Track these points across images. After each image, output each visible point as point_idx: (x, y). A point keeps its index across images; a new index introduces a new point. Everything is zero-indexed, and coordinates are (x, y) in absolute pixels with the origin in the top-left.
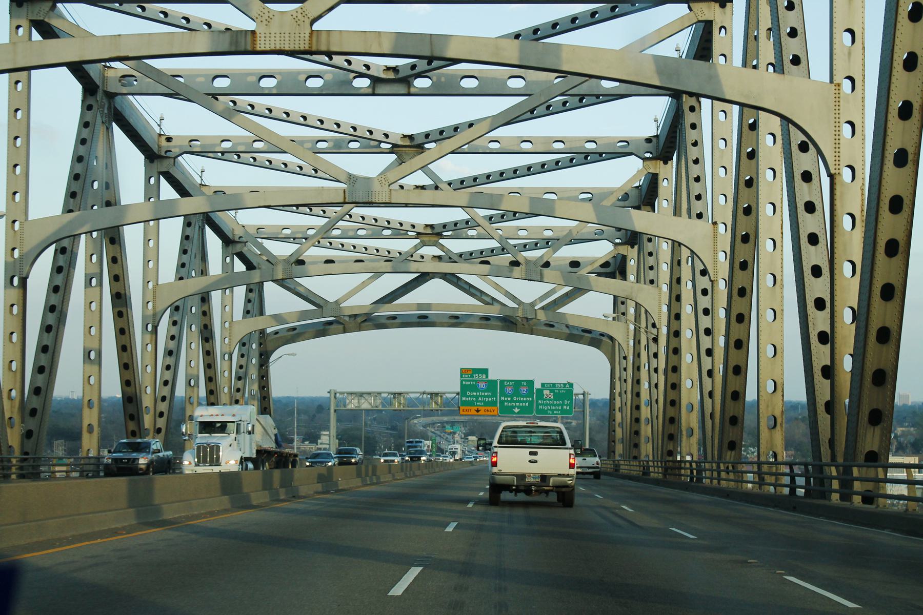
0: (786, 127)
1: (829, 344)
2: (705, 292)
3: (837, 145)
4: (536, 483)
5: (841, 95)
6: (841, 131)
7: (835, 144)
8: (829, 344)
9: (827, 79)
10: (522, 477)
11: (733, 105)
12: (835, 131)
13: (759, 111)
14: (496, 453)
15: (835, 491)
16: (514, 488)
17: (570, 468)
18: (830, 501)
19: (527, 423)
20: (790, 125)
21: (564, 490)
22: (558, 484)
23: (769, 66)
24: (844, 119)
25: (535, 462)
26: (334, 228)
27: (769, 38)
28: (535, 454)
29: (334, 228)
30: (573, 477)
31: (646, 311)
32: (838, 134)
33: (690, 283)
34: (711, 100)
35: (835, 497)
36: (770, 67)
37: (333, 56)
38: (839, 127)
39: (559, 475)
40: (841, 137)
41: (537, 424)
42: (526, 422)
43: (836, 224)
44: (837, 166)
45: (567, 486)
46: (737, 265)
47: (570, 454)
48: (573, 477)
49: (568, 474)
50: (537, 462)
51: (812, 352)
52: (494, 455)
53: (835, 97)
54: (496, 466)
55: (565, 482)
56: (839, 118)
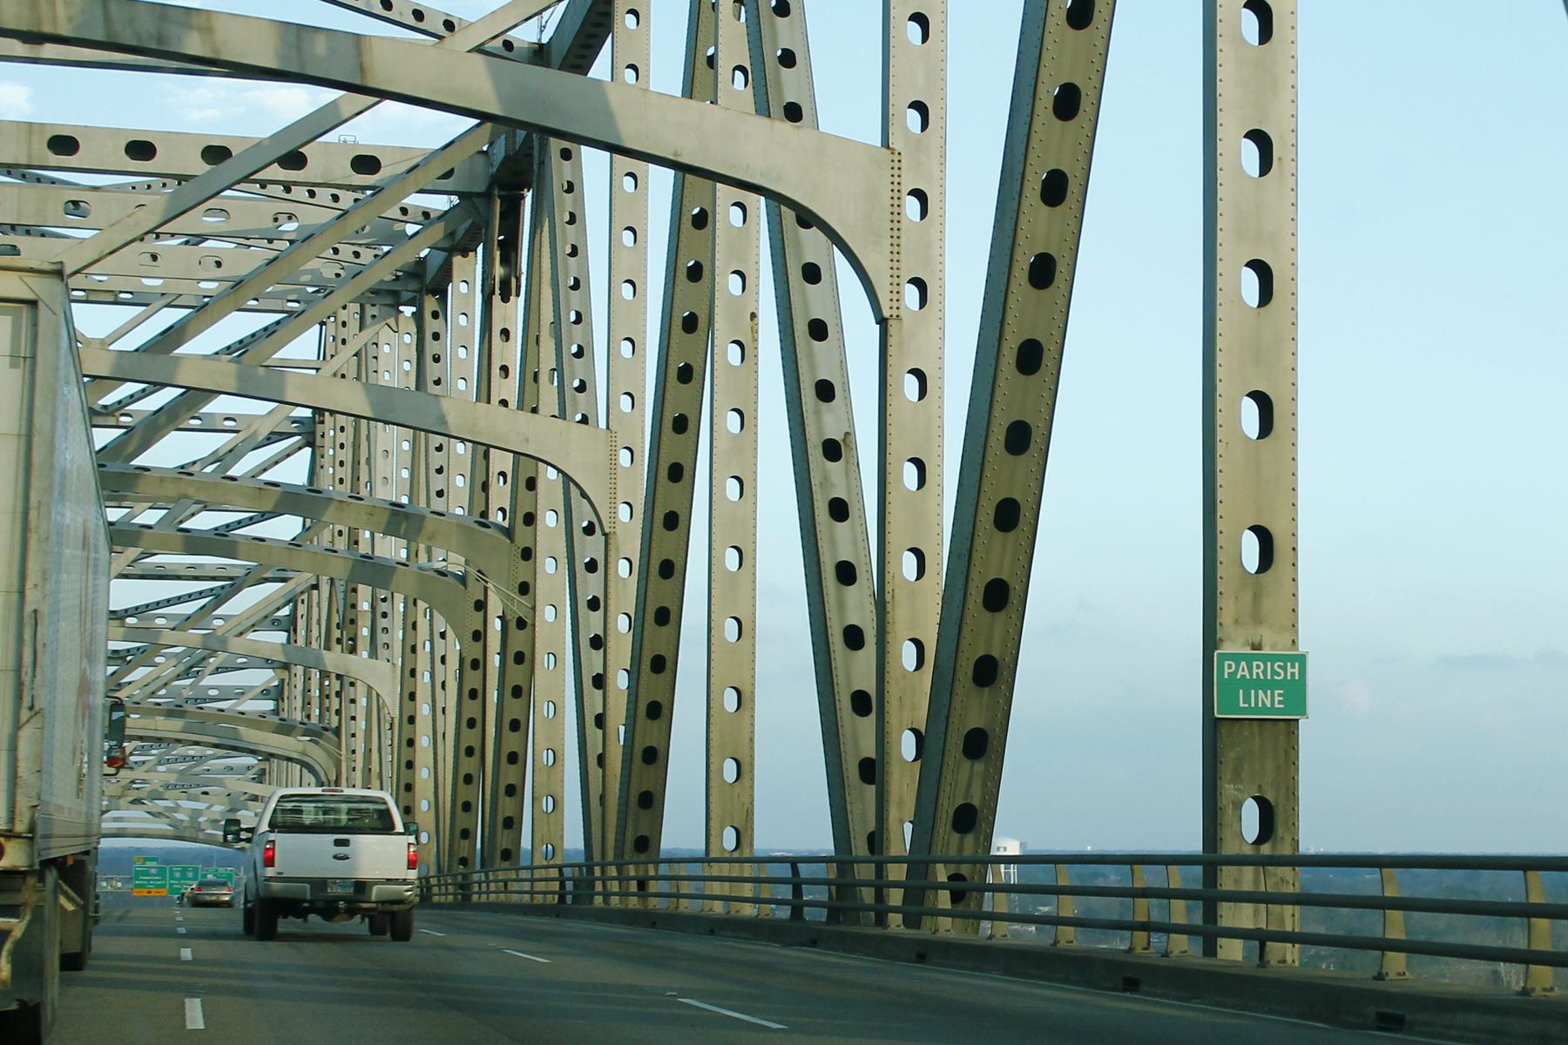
0: (777, 210)
1: (873, 715)
2: (594, 604)
3: (895, 262)
4: (344, 897)
5: (903, 225)
6: (902, 206)
7: (892, 205)
8: (873, 715)
9: (877, 141)
10: (320, 884)
11: (650, 165)
12: (892, 229)
13: (718, 185)
14: (273, 842)
15: (895, 910)
16: (306, 905)
17: (409, 869)
18: (886, 929)
19: (323, 791)
20: (784, 208)
21: (395, 907)
22: (385, 897)
23: (737, 72)
24: (907, 188)
25: (345, 858)
26: (122, 412)
27: (737, 14)
28: (345, 843)
29: (122, 412)
30: (412, 884)
31: (378, 695)
32: (896, 212)
33: (427, 675)
34: (609, 153)
35: (895, 920)
36: (738, 73)
37: (292, 187)
38: (899, 229)
39: (389, 881)
40: (902, 218)
41: (342, 791)
42: (322, 788)
43: (890, 478)
44: (895, 262)
45: (400, 902)
46: (464, 723)
47: (409, 844)
48: (412, 884)
49: (405, 880)
50: (347, 858)
51: (888, 390)
52: (268, 846)
53: (892, 183)
54: (272, 865)
55: (400, 893)
56: (899, 184)
